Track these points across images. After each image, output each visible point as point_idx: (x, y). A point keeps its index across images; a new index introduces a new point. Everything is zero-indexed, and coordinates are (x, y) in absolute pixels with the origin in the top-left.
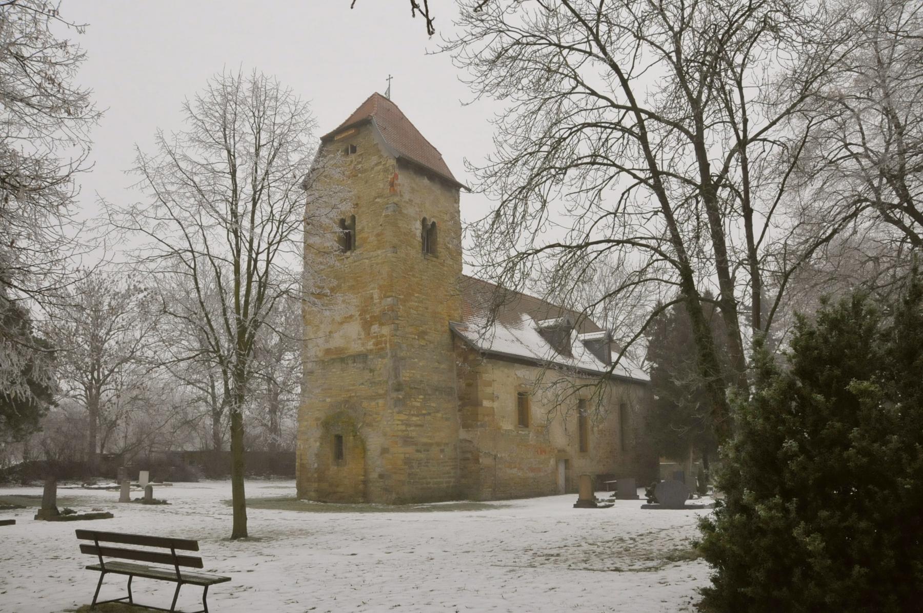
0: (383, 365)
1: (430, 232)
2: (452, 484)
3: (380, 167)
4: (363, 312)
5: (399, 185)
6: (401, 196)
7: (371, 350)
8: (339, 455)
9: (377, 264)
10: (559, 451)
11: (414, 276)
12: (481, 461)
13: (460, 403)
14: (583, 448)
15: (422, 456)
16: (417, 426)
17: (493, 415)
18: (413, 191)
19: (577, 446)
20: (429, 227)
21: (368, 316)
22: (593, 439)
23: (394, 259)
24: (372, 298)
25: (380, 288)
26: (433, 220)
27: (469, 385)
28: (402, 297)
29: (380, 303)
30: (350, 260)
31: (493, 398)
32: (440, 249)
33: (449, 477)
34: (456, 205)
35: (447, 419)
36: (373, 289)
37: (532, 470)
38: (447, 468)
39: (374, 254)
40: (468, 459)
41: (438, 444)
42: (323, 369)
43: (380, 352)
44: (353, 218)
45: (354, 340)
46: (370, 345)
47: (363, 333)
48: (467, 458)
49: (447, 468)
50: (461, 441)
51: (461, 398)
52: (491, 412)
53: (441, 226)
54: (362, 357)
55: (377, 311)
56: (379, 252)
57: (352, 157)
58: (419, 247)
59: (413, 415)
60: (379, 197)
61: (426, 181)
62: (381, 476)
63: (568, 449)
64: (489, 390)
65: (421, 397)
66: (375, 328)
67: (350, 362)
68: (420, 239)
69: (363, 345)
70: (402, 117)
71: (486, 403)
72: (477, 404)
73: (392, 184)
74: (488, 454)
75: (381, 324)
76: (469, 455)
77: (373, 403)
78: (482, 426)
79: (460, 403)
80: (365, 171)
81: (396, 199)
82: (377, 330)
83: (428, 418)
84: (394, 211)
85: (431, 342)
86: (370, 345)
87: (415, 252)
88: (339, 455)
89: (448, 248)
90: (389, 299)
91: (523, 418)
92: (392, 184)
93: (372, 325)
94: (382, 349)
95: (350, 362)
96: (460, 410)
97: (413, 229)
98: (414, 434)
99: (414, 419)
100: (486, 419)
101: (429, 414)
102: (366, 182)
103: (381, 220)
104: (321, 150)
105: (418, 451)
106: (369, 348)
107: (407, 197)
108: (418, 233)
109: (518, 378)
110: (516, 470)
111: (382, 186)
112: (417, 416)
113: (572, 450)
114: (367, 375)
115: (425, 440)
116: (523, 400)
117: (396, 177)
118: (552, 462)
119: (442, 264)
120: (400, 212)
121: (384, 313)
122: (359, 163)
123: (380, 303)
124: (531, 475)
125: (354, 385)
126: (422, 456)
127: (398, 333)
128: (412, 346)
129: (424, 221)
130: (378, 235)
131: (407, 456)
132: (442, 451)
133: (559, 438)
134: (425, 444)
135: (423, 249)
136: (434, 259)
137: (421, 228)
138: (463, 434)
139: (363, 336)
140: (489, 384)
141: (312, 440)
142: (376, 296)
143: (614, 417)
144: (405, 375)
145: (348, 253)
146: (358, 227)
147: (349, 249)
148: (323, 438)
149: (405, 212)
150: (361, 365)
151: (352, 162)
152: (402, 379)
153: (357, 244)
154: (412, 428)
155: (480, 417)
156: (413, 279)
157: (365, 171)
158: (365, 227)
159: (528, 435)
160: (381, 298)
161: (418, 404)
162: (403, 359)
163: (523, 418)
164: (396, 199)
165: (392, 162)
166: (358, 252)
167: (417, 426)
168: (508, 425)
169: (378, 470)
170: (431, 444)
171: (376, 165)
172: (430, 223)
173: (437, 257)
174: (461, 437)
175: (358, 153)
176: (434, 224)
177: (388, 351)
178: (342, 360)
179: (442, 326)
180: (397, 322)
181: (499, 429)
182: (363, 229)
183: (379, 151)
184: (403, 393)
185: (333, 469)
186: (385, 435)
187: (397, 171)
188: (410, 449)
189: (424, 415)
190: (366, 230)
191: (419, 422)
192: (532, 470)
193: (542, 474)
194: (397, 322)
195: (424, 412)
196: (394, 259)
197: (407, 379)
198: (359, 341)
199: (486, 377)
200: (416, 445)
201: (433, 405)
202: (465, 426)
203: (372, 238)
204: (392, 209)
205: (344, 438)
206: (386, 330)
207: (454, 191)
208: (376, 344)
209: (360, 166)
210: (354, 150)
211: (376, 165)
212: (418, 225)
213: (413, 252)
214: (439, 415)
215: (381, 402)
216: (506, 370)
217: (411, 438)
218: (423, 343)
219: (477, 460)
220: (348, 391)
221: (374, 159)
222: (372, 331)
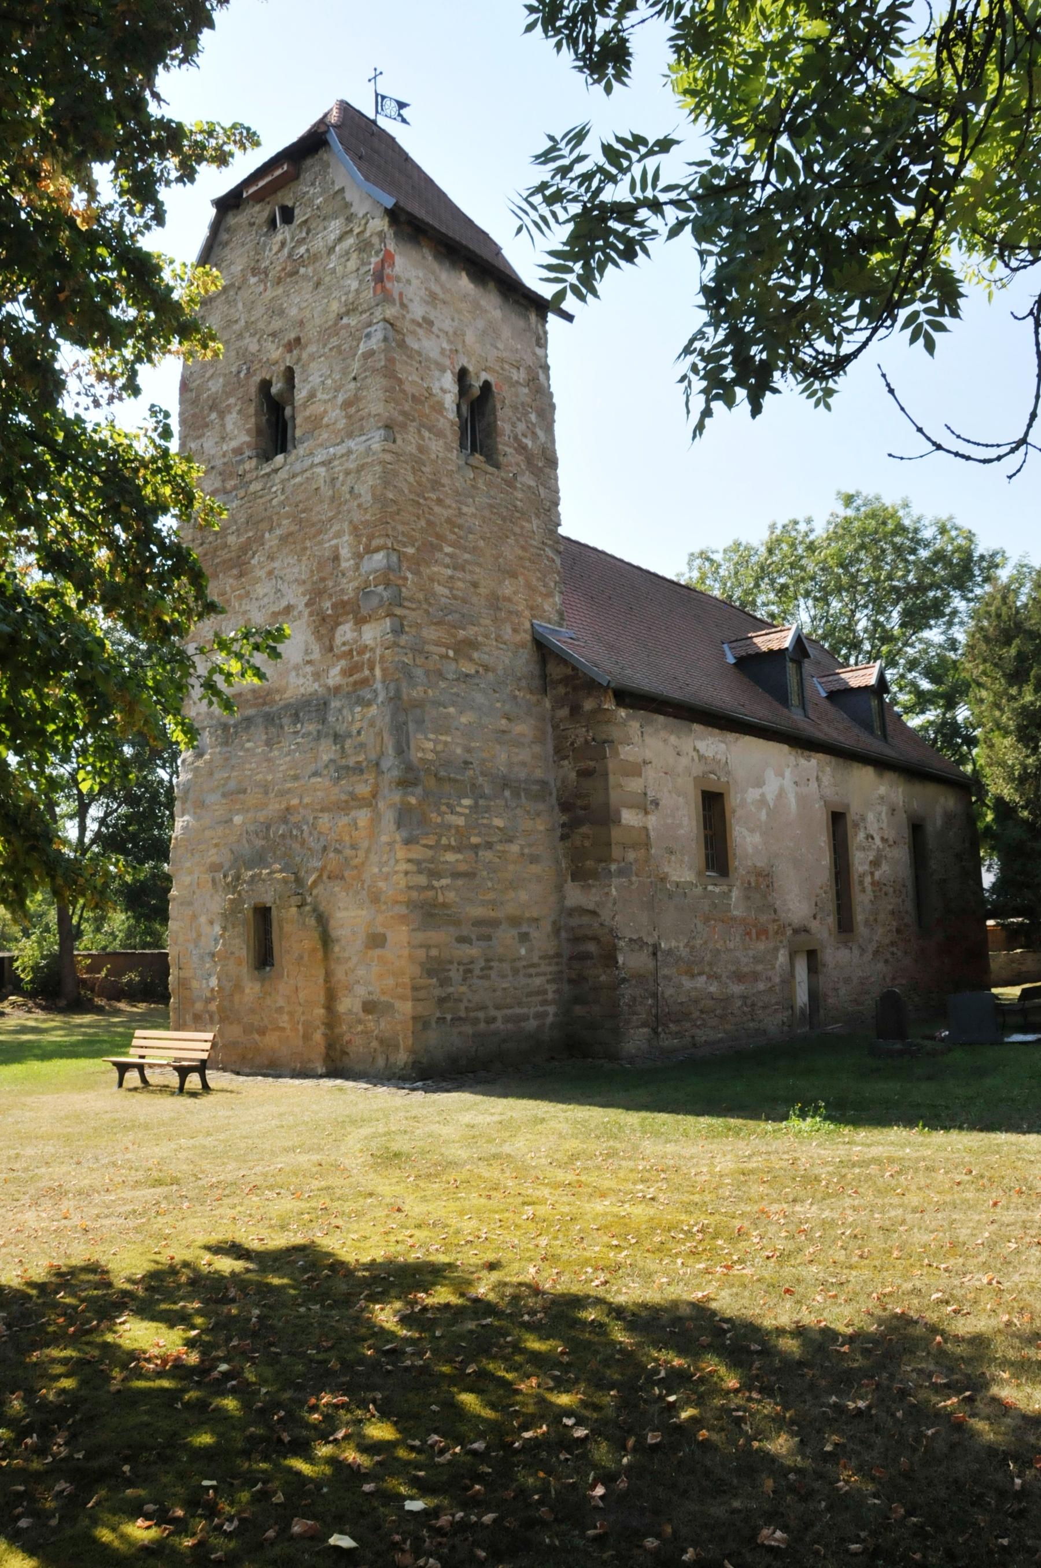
0: (367, 721)
1: (477, 409)
2: (550, 1019)
3: (350, 241)
4: (316, 594)
5: (398, 279)
6: (403, 306)
7: (337, 689)
8: (264, 957)
9: (348, 473)
10: (796, 931)
11: (439, 502)
12: (621, 960)
13: (564, 818)
14: (845, 924)
15: (473, 951)
16: (456, 875)
17: (647, 845)
18: (433, 299)
19: (831, 920)
20: (476, 392)
21: (327, 604)
22: (862, 901)
23: (388, 457)
24: (336, 558)
25: (355, 530)
26: (484, 376)
27: (585, 774)
28: (410, 550)
29: (357, 567)
30: (283, 474)
31: (646, 804)
32: (505, 447)
33: (545, 1003)
34: (539, 351)
35: (534, 859)
36: (338, 535)
37: (739, 977)
38: (538, 981)
39: (341, 450)
40: (585, 956)
41: (515, 921)
42: (226, 743)
43: (356, 692)
44: (289, 375)
45: (297, 668)
46: (334, 676)
47: (316, 648)
48: (585, 955)
49: (538, 981)
50: (571, 912)
51: (565, 807)
52: (643, 840)
53: (503, 393)
54: (314, 708)
55: (349, 587)
56: (351, 444)
57: (283, 232)
58: (452, 437)
59: (449, 848)
60: (347, 313)
61: (464, 283)
62: (369, 1007)
63: (814, 925)
64: (634, 785)
65: (466, 802)
66: (345, 632)
67: (286, 721)
68: (452, 415)
69: (317, 676)
70: (407, 158)
71: (629, 817)
72: (607, 818)
73: (379, 277)
74: (638, 943)
75: (360, 621)
76: (592, 947)
77: (345, 820)
78: (621, 872)
79: (564, 818)
80: (314, 258)
81: (391, 312)
82: (350, 636)
83: (486, 855)
84: (385, 339)
85: (487, 669)
86: (334, 676)
87: (442, 446)
88: (264, 957)
89: (524, 447)
90: (379, 556)
91: (717, 853)
92: (379, 277)
93: (338, 624)
94: (365, 682)
95: (286, 721)
96: (563, 838)
97: (436, 390)
98: (451, 896)
99: (450, 857)
100: (631, 856)
101: (489, 846)
102: (318, 285)
103: (356, 366)
104: (216, 227)
105: (462, 940)
106: (331, 682)
107: (418, 310)
108: (450, 400)
109: (701, 757)
110: (704, 978)
111: (354, 285)
112: (458, 850)
113: (823, 929)
114: (327, 752)
115: (478, 912)
116: (713, 805)
117: (388, 259)
118: (782, 957)
119: (510, 483)
120: (402, 345)
121: (364, 592)
122: (301, 242)
123: (357, 567)
124: (737, 989)
125: (296, 778)
126: (473, 951)
127: (403, 640)
128: (441, 675)
129: (462, 376)
130: (347, 404)
131: (434, 952)
132: (524, 937)
133: (800, 898)
134: (478, 923)
135: (462, 446)
136: (490, 469)
137: (455, 389)
138: (575, 896)
139: (316, 655)
140: (635, 770)
141: (203, 919)
142: (345, 552)
143: (901, 854)
144: (425, 746)
145: (280, 458)
146: (301, 394)
147: (283, 449)
148: (230, 915)
149: (416, 346)
150: (312, 728)
151: (283, 244)
152: (415, 755)
153: (298, 433)
154: (444, 882)
155: (616, 852)
156: (437, 509)
157: (314, 258)
158: (318, 392)
159: (727, 895)
160: (359, 557)
161: (461, 821)
162: (418, 705)
163: (717, 853)
164: (391, 312)
165: (380, 224)
166: (301, 450)
167: (456, 875)
168: (683, 869)
169: (361, 991)
170: (495, 923)
171: (340, 239)
172: (477, 384)
173: (497, 466)
174: (570, 903)
175: (298, 221)
176: (487, 386)
177: (378, 686)
178: (270, 720)
179: (515, 631)
180: (398, 611)
181: (663, 879)
182: (312, 395)
183: (348, 205)
184: (419, 790)
185: (251, 989)
186: (375, 898)
187: (391, 246)
188: (441, 936)
189: (476, 847)
190: (320, 395)
191: (463, 868)
192: (739, 977)
193: (761, 986)
194: (398, 611)
195: (475, 840)
196: (388, 457)
197: (430, 756)
198: (309, 669)
199: (628, 753)
200: (457, 923)
201: (498, 822)
202: (579, 875)
203: (335, 415)
204: (379, 335)
205: (274, 912)
206: (372, 634)
207: (533, 318)
208: (348, 672)
209: (302, 250)
210: (288, 215)
211: (340, 239)
212: (448, 382)
213: (436, 446)
214: (515, 848)
215: (363, 816)
216: (673, 739)
217: (444, 905)
218: (468, 668)
219: (610, 958)
220: (282, 794)
221: (335, 226)
222: (338, 640)
